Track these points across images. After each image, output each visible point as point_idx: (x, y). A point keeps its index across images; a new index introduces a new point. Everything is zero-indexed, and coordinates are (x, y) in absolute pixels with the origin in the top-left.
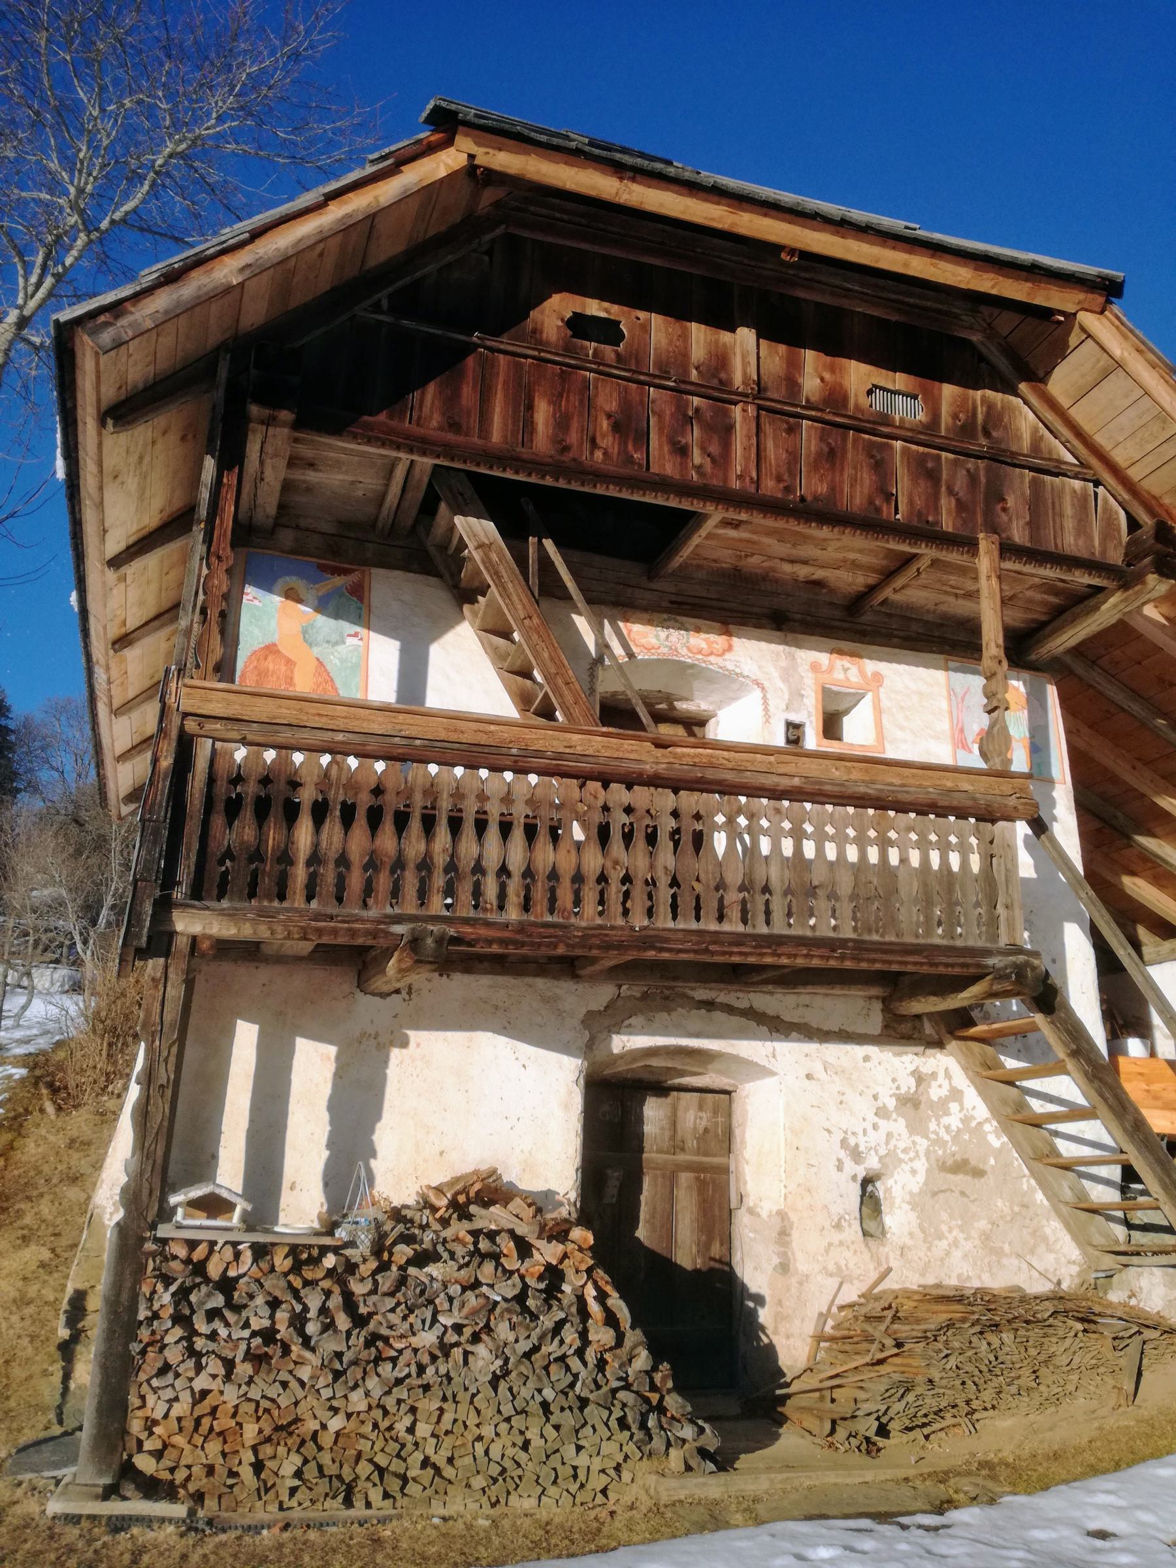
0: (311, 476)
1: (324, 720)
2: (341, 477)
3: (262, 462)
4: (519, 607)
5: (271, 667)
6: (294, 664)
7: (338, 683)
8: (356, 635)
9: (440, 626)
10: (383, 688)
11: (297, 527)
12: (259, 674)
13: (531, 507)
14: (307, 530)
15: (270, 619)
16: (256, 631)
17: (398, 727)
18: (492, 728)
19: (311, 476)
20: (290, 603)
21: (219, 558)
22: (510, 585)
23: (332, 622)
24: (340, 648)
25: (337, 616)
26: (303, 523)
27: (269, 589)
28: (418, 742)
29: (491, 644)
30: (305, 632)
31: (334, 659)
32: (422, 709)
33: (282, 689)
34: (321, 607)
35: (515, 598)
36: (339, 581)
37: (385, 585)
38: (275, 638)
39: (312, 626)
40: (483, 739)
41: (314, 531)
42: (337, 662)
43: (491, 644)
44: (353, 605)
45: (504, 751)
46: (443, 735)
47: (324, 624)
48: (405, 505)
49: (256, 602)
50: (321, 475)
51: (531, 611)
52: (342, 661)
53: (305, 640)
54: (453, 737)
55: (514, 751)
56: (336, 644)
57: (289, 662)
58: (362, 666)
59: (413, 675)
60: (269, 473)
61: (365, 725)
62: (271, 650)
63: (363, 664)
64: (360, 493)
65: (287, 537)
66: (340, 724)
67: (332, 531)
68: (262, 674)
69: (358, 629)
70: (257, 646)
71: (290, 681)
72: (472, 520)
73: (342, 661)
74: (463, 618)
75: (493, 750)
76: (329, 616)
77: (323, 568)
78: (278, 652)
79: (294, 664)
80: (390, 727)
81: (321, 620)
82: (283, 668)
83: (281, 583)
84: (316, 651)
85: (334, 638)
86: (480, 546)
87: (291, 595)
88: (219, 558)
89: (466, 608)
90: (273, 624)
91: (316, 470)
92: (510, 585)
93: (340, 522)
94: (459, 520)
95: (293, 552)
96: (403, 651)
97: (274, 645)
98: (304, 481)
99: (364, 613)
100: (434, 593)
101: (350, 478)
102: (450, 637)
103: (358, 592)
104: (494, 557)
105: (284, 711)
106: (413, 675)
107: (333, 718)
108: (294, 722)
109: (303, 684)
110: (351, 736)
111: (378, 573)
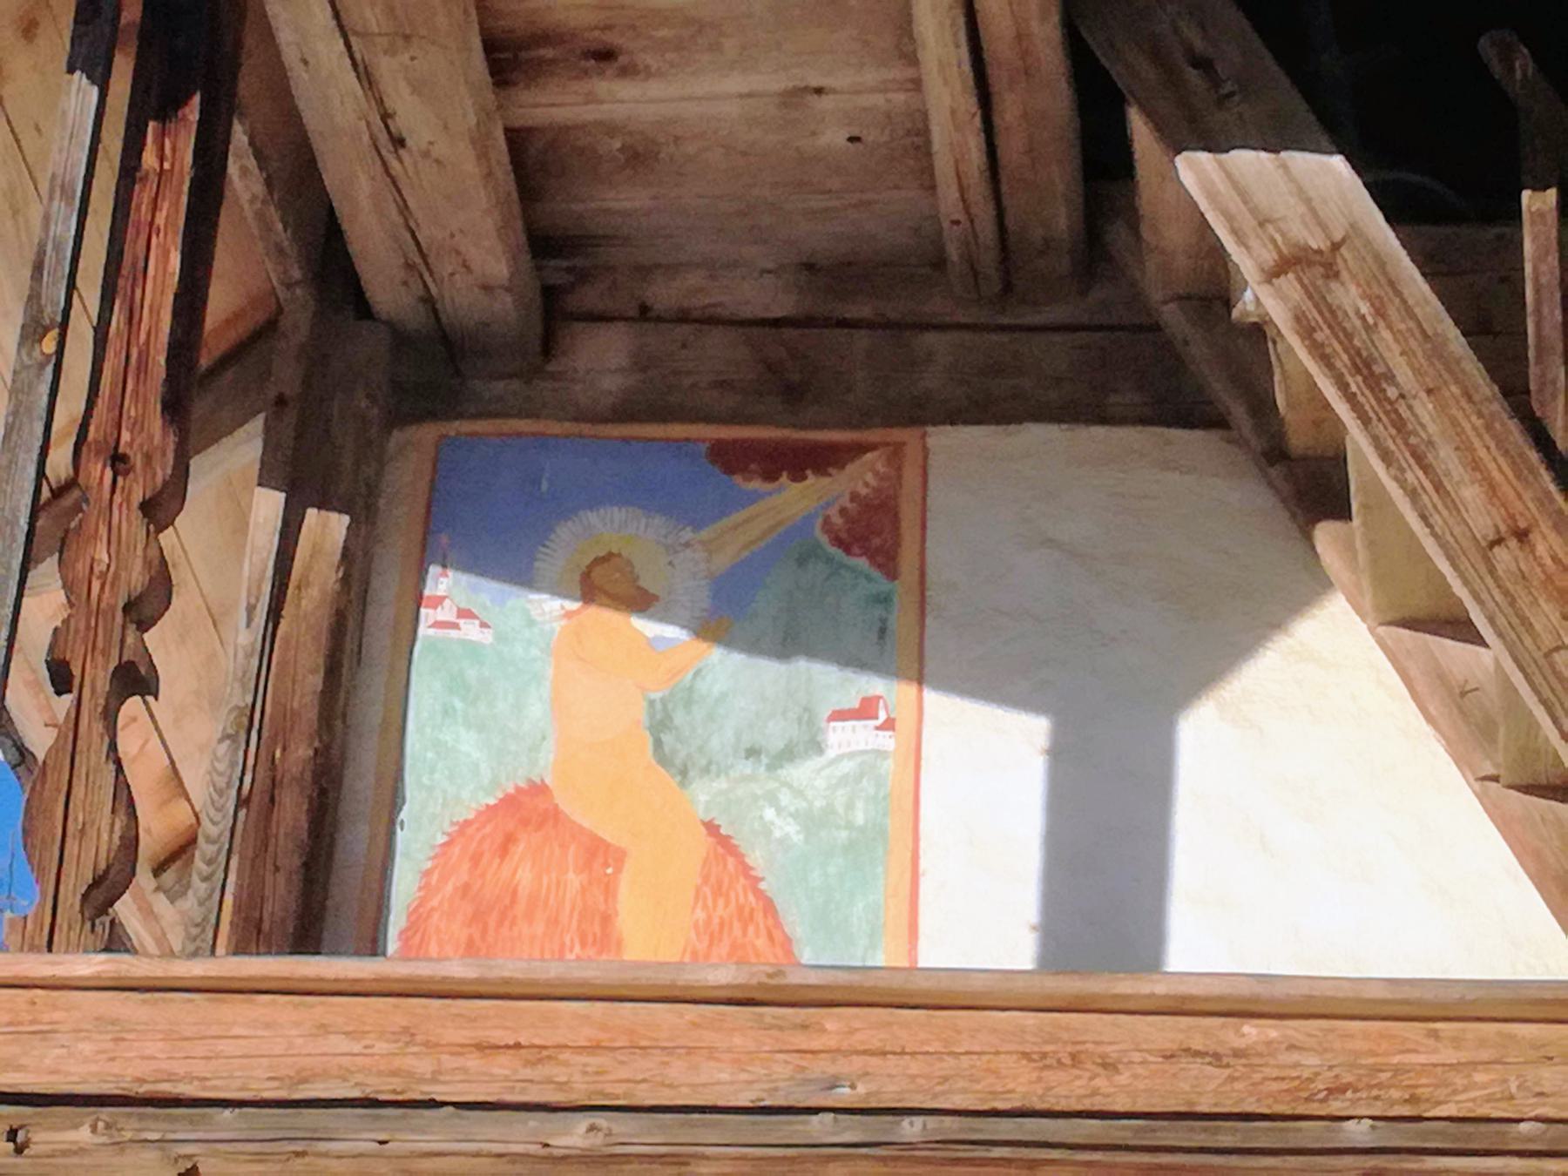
0: (619, 101)
1: (503, 1065)
2: (735, 83)
3: (365, 75)
4: (1470, 493)
5: (525, 877)
6: (616, 856)
7: (796, 922)
8: (866, 710)
9: (1222, 629)
10: (981, 907)
11: (644, 313)
12: (478, 917)
13: (1523, 64)
14: (683, 317)
15: (518, 688)
16: (468, 744)
17: (822, 1067)
18: (1251, 1031)
19: (619, 101)
20: (604, 617)
21: (118, 461)
22: (1425, 409)
23: (768, 673)
24: (800, 772)
25: (787, 642)
26: (664, 294)
27: (522, 576)
28: (911, 1129)
29: (1440, 677)
30: (660, 724)
31: (776, 821)
32: (1160, 988)
33: (577, 963)
34: (722, 620)
35: (1447, 458)
36: (799, 500)
37: (992, 490)
38: (544, 766)
39: (689, 698)
40: (1206, 1088)
41: (711, 320)
42: (790, 829)
43: (1440, 677)
44: (862, 593)
45: (1309, 1134)
46: (1021, 1087)
47: (736, 683)
48: (1012, 149)
49: (470, 631)
50: (655, 88)
51: (1527, 508)
52: (812, 822)
53: (662, 756)
54: (1068, 1090)
55: (1358, 1132)
56: (788, 755)
57: (600, 856)
58: (892, 837)
59: (1107, 853)
60: (411, 115)
61: (677, 1070)
62: (526, 811)
63: (912, 824)
64: (834, 137)
65: (602, 358)
66: (574, 1078)
67: (783, 306)
68: (489, 914)
69: (875, 685)
70: (474, 797)
71: (601, 928)
72: (1246, 161)
73: (812, 822)
74: (1321, 584)
75: (1261, 1134)
76: (753, 647)
77: (730, 458)
78: (554, 816)
79: (616, 856)
80: (782, 1069)
81: (727, 672)
82: (574, 880)
83: (569, 542)
84: (704, 796)
85: (776, 734)
86: (1290, 262)
87: (607, 584)
88: (118, 461)
89: (1325, 534)
90: (537, 710)
91: (627, 72)
92: (1425, 409)
93: (810, 267)
94: (1195, 170)
95: (625, 412)
96: (1059, 754)
97: (538, 789)
98: (611, 129)
99: (901, 619)
100: (1186, 486)
101: (772, 81)
102: (1269, 672)
103: (873, 533)
104: (1349, 297)
105: (339, 1044)
106: (1107, 853)
107: (541, 1054)
108: (383, 1088)
109: (654, 930)
110: (623, 1126)
111: (953, 447)
